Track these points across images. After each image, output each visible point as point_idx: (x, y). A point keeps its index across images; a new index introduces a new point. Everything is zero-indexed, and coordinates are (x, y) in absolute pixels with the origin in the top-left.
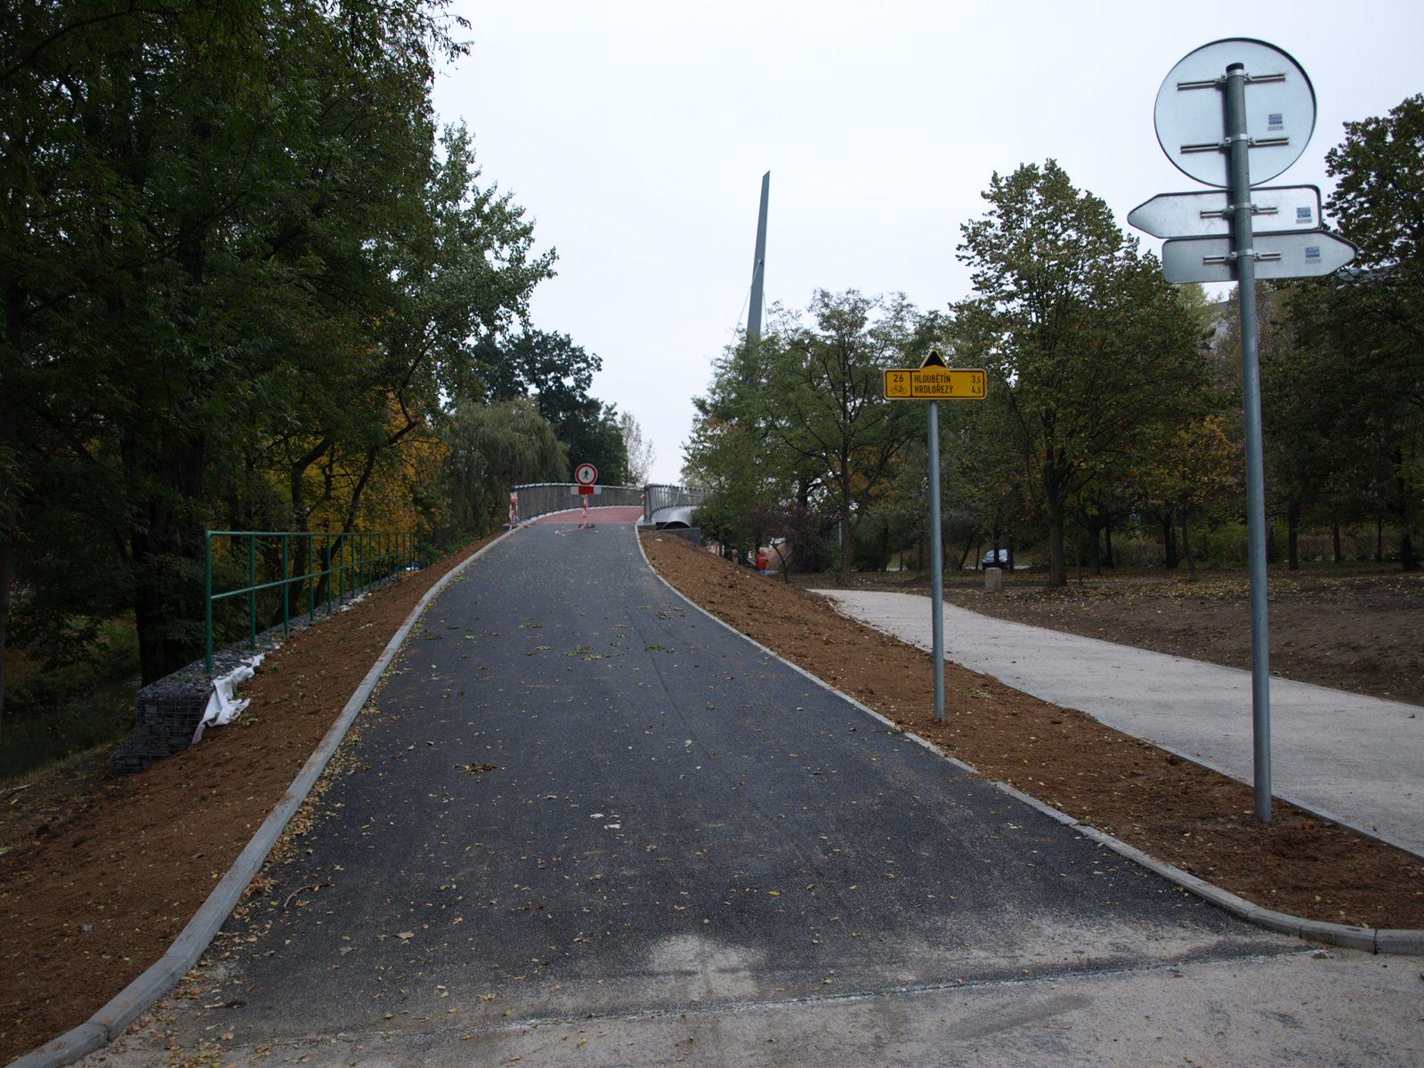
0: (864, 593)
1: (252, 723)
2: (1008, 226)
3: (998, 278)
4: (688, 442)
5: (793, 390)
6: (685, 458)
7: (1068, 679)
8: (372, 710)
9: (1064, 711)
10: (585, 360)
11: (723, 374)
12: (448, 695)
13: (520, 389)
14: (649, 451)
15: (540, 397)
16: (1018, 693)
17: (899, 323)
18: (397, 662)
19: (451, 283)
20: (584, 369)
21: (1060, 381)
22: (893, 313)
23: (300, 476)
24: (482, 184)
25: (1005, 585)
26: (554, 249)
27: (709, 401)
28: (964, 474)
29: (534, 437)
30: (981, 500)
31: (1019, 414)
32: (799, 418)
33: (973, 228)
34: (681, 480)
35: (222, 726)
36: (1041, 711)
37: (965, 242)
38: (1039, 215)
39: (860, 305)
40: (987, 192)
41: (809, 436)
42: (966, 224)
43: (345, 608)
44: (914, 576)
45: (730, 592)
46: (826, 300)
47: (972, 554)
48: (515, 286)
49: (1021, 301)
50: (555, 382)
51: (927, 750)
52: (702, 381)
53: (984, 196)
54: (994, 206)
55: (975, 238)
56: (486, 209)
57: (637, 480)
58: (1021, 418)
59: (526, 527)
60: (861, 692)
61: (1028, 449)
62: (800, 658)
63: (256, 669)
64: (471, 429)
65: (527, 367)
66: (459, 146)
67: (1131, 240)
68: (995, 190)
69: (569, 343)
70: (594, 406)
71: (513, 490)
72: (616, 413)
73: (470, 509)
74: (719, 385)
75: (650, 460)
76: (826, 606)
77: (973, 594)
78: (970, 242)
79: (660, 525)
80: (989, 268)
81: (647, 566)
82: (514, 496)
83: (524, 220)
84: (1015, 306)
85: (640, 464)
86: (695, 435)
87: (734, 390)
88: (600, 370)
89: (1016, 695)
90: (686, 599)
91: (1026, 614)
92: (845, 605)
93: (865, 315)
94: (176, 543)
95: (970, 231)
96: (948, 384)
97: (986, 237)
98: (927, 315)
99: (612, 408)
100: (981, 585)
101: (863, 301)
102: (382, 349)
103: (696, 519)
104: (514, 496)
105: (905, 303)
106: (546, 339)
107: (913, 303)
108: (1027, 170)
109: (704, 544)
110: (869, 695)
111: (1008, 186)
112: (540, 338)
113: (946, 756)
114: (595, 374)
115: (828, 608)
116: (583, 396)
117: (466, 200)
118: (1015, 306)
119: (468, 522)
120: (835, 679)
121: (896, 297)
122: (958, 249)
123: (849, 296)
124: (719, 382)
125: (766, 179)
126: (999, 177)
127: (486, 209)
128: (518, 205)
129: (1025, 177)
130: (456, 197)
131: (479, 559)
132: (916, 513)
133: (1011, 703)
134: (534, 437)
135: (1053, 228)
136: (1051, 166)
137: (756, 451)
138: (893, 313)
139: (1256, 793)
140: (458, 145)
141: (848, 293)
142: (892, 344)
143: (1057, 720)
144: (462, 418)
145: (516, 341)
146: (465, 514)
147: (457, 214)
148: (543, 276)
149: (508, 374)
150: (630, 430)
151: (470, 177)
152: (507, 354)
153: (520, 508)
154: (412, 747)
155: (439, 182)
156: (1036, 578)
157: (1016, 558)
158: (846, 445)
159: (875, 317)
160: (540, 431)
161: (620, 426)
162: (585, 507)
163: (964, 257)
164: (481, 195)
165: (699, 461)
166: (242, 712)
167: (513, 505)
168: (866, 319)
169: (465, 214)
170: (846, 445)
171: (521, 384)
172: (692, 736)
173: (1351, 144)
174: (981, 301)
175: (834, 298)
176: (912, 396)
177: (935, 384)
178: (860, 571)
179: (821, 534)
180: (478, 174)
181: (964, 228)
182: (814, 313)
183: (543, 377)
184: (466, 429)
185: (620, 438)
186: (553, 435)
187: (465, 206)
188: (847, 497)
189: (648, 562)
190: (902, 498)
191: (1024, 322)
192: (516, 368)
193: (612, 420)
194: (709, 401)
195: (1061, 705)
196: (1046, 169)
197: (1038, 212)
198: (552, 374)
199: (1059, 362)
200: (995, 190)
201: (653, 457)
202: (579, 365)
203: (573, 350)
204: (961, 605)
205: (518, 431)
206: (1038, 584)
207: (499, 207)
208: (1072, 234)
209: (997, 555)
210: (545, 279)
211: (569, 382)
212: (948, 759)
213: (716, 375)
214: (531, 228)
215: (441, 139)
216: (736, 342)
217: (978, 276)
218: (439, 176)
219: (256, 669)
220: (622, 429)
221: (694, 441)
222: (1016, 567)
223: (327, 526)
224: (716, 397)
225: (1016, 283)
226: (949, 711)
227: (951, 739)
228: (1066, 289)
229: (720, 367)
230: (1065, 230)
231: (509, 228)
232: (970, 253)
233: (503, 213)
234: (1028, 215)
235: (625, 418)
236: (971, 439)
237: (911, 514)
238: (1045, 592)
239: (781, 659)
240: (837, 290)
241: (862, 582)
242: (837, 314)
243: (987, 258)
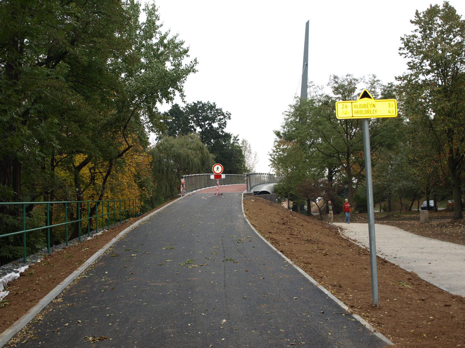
0: (359, 224)
1: (6, 305)
2: (425, 37)
3: (421, 63)
4: (271, 152)
5: (321, 124)
6: (270, 160)
7: (459, 273)
8: (59, 300)
9: (453, 297)
10: (223, 115)
11: (288, 119)
12: (105, 291)
13: (192, 129)
14: (255, 157)
15: (201, 133)
16: (428, 284)
17: (373, 90)
18: (88, 272)
19: (146, 77)
20: (222, 119)
21: (455, 114)
22: (370, 85)
23: (78, 174)
24: (163, 30)
25: (431, 218)
26: (196, 58)
27: (282, 132)
28: (410, 163)
30: (419, 176)
31: (434, 131)
32: (325, 138)
33: (407, 39)
36: (439, 297)
38: (428, 9)
39: (353, 81)
40: (413, 20)
41: (330, 146)
42: (403, 37)
43: (89, 238)
44: (386, 214)
45: (283, 227)
46: (336, 80)
47: (416, 202)
48: (175, 79)
49: (433, 74)
50: (208, 126)
51: (364, 327)
52: (279, 123)
53: (412, 22)
54: (417, 27)
55: (408, 44)
56: (166, 41)
58: (435, 133)
59: (189, 195)
60: (335, 286)
61: (440, 150)
62: (306, 266)
63: (21, 274)
64: (168, 149)
65: (195, 119)
66: (152, 13)
68: (418, 19)
69: (215, 107)
71: (182, 178)
72: (238, 140)
73: (168, 187)
74: (287, 124)
75: (256, 161)
76: (336, 232)
77: (414, 224)
78: (405, 46)
79: (256, 193)
80: (415, 58)
81: (242, 214)
83: (184, 46)
84: (430, 77)
85: (251, 164)
86: (275, 149)
87: (294, 126)
88: (230, 119)
89: (427, 286)
90: (256, 232)
91: (440, 234)
92: (347, 231)
93: (356, 86)
94: (7, 208)
95: (406, 40)
96: (374, 109)
97: (414, 43)
99: (236, 137)
100: (418, 219)
101: (355, 80)
102: (114, 112)
103: (276, 190)
104: (183, 180)
105: (376, 79)
106: (204, 105)
107: (379, 79)
108: (434, 7)
109: (280, 202)
110: (338, 288)
111: (424, 16)
112: (201, 105)
113: (375, 331)
115: (337, 233)
116: (222, 132)
117: (156, 38)
118: (430, 77)
119: (168, 193)
120: (321, 278)
121: (371, 76)
122: (400, 49)
123: (348, 77)
124: (286, 122)
125: (307, 24)
126: (419, 12)
127: (166, 41)
128: (181, 40)
129: (433, 12)
130: (151, 37)
131: (160, 212)
132: (385, 183)
133: (423, 291)
135: (448, 36)
136: (446, 5)
137: (305, 155)
138: (370, 85)
140: (151, 12)
141: (347, 76)
143: (448, 304)
144: (164, 144)
145: (190, 107)
146: (166, 190)
147: (151, 45)
148: (191, 72)
149: (187, 121)
150: (246, 147)
151: (158, 27)
152: (186, 113)
153: (186, 186)
154: (67, 324)
155: (143, 30)
156: (449, 214)
157: (438, 204)
158: (348, 150)
161: (241, 145)
162: (217, 185)
163: (403, 54)
164: (163, 35)
165: (279, 162)
166: (4, 299)
167: (183, 185)
168: (356, 88)
169: (156, 45)
170: (348, 150)
171: (193, 127)
172: (228, 317)
174: (411, 75)
175: (340, 79)
176: (353, 117)
177: (366, 109)
178: (360, 212)
180: (161, 25)
181: (402, 39)
182: (330, 86)
183: (203, 123)
184: (165, 149)
185: (241, 151)
187: (155, 41)
188: (350, 176)
189: (243, 211)
190: (378, 176)
191: (436, 84)
192: (190, 119)
194: (282, 132)
195: (452, 293)
196: (444, 6)
197: (441, 29)
198: (208, 122)
199: (454, 104)
200: (418, 19)
201: (257, 160)
202: (220, 117)
203: (217, 110)
204: (407, 230)
205: (191, 149)
206: (449, 218)
207: (172, 41)
208: (459, 39)
209: (428, 203)
210: (191, 74)
211: (215, 125)
212: (375, 334)
213: (285, 119)
214: (188, 50)
215: (143, 9)
216: (294, 102)
217: (410, 63)
218: (143, 27)
219: (21, 274)
220: (241, 147)
221: (274, 152)
222: (439, 209)
223: (93, 197)
224: (285, 130)
225: (430, 65)
226: (382, 298)
227: (381, 318)
228: (457, 67)
229: (287, 115)
230: (455, 37)
231: (177, 51)
232: (406, 51)
233: (174, 44)
234: (435, 30)
235: (243, 142)
236: (413, 146)
237: (384, 184)
238: (451, 222)
239: (295, 266)
240: (342, 76)
241: (359, 218)
242: (342, 86)
243: (415, 53)
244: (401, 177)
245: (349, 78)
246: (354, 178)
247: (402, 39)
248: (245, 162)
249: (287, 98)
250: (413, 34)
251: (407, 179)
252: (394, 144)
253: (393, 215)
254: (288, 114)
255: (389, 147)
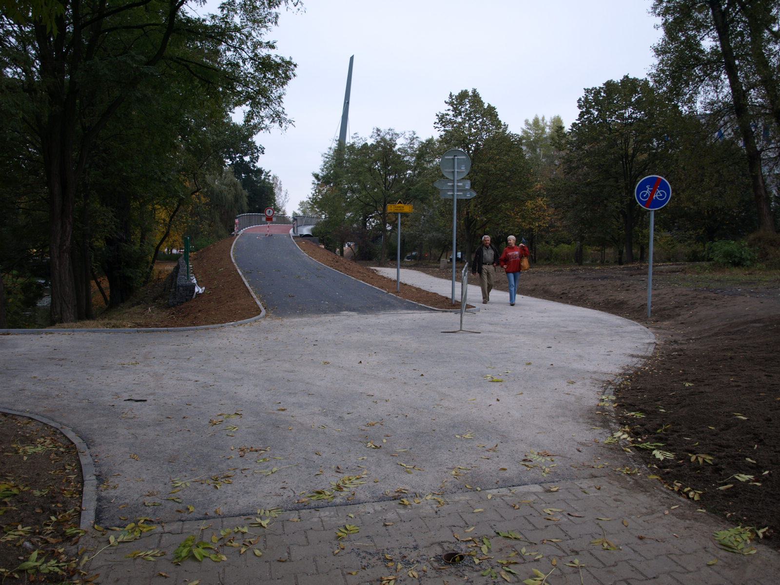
10: (256, 148)
14: (286, 195)
17: (411, 146)
29: (232, 188)
34: (299, 209)
35: (200, 294)
37: (437, 121)
40: (447, 101)
52: (317, 164)
53: (446, 103)
57: (280, 210)
67: (505, 125)
70: (260, 171)
71: (236, 218)
72: (270, 176)
75: (286, 200)
78: (439, 121)
82: (237, 221)
85: (281, 202)
88: (263, 154)
98: (425, 142)
99: (268, 173)
101: (396, 134)
104: (237, 221)
105: (415, 136)
114: (261, 156)
116: (254, 166)
121: (411, 133)
125: (352, 59)
126: (453, 94)
129: (463, 95)
134: (232, 188)
136: (474, 91)
139: (452, 299)
142: (408, 155)
150: (276, 184)
159: (400, 143)
160: (235, 185)
161: (271, 182)
163: (437, 127)
173: (586, 98)
179: (373, 241)
181: (438, 115)
186: (241, 188)
193: (268, 179)
194: (320, 175)
205: (224, 185)
211: (247, 159)
220: (273, 184)
229: (327, 158)
232: (439, 126)
240: (384, 128)
244: (432, 229)
245: (391, 132)
246: (388, 225)
247: (438, 115)
248: (275, 201)
249: (328, 142)
250: (447, 112)
251: (438, 230)
252: (427, 198)
253: (422, 264)
254: (326, 156)
255: (422, 200)
